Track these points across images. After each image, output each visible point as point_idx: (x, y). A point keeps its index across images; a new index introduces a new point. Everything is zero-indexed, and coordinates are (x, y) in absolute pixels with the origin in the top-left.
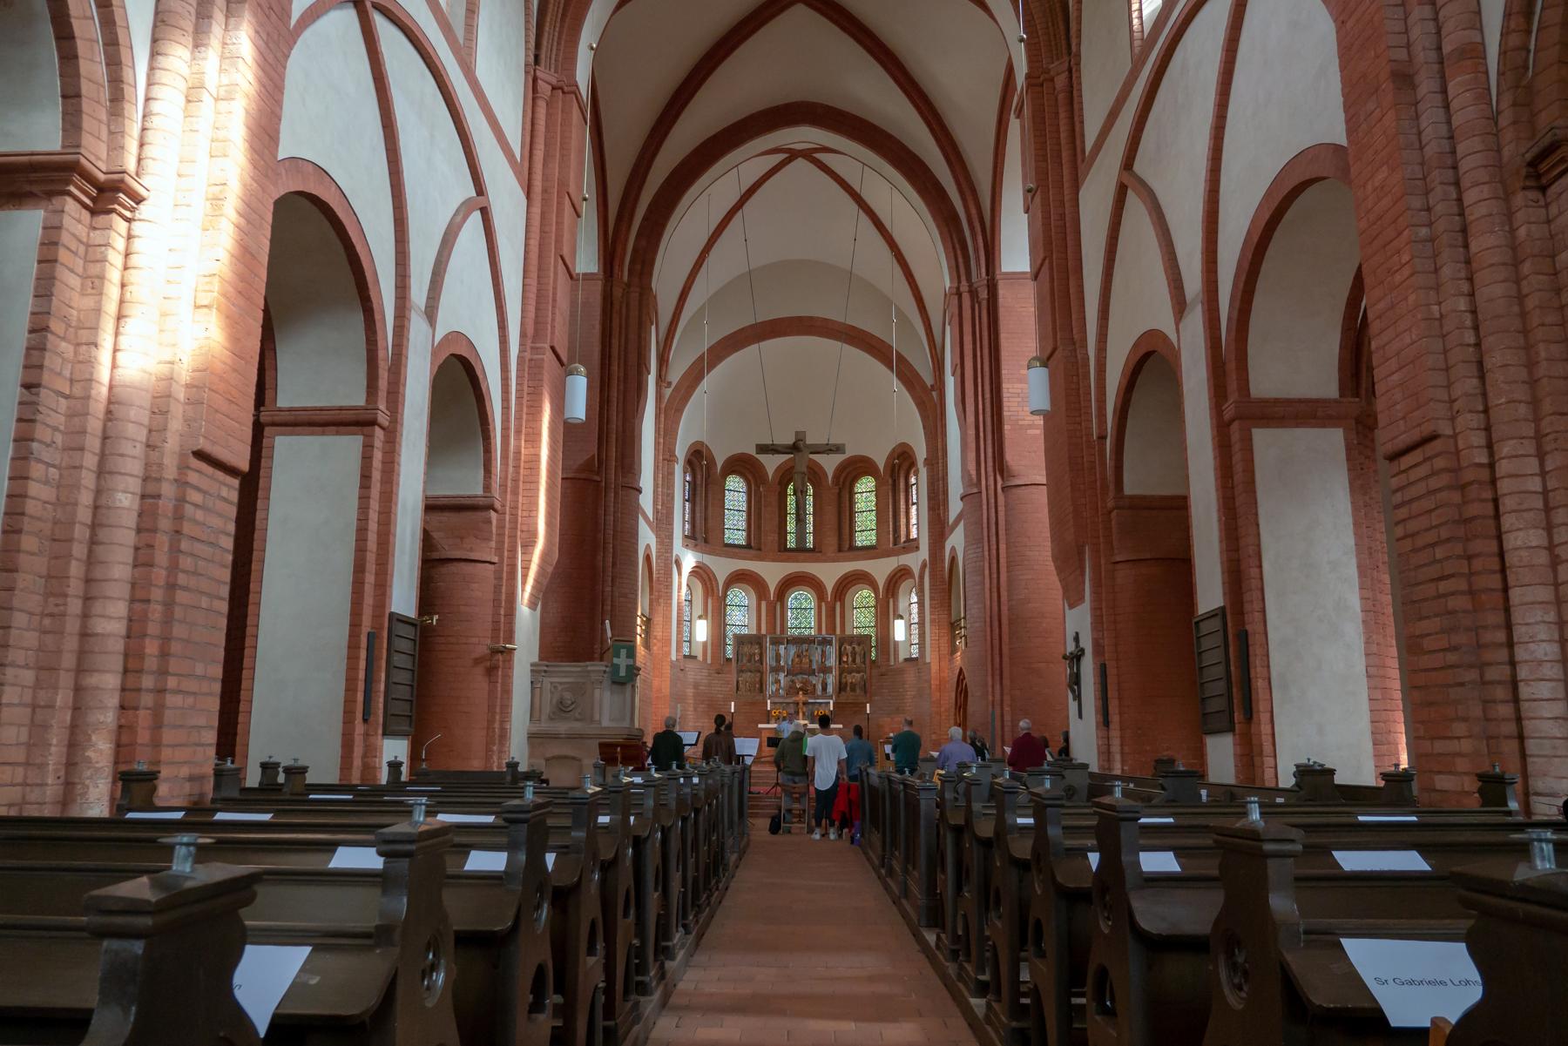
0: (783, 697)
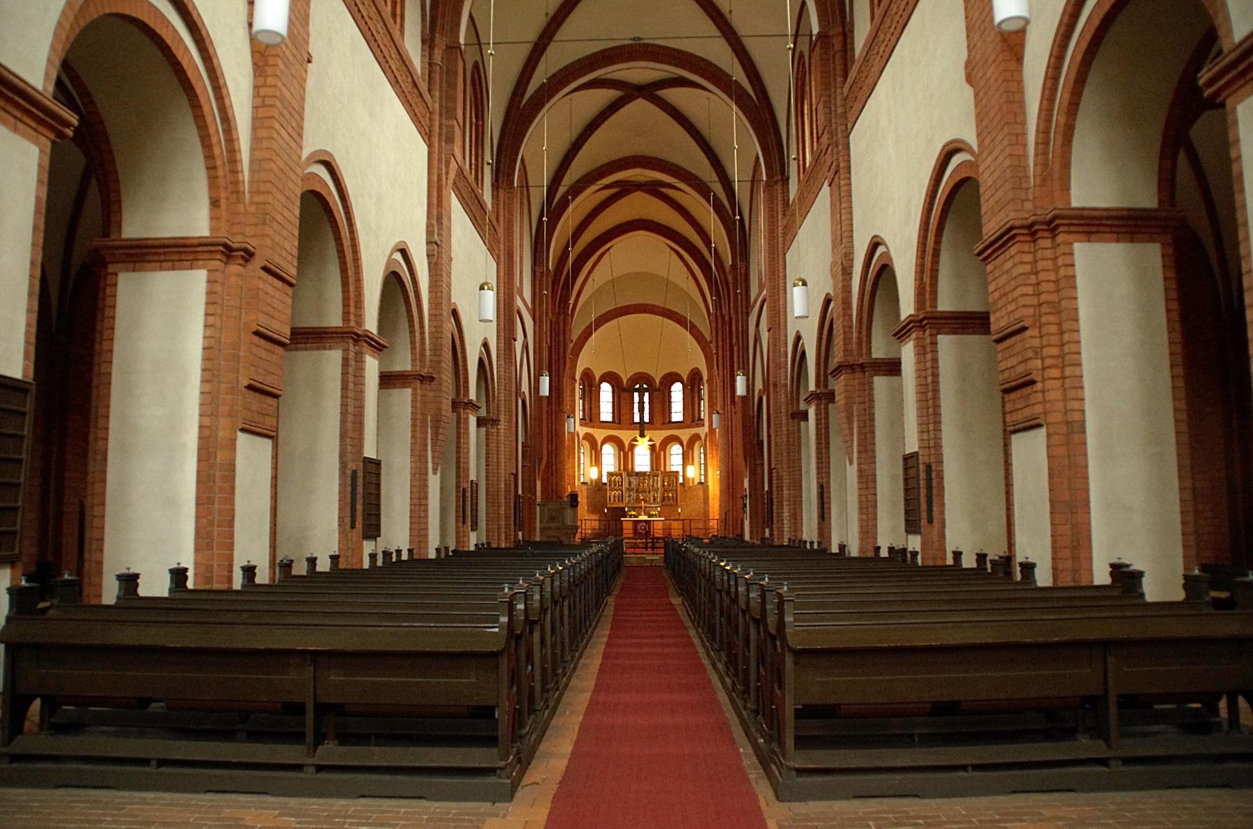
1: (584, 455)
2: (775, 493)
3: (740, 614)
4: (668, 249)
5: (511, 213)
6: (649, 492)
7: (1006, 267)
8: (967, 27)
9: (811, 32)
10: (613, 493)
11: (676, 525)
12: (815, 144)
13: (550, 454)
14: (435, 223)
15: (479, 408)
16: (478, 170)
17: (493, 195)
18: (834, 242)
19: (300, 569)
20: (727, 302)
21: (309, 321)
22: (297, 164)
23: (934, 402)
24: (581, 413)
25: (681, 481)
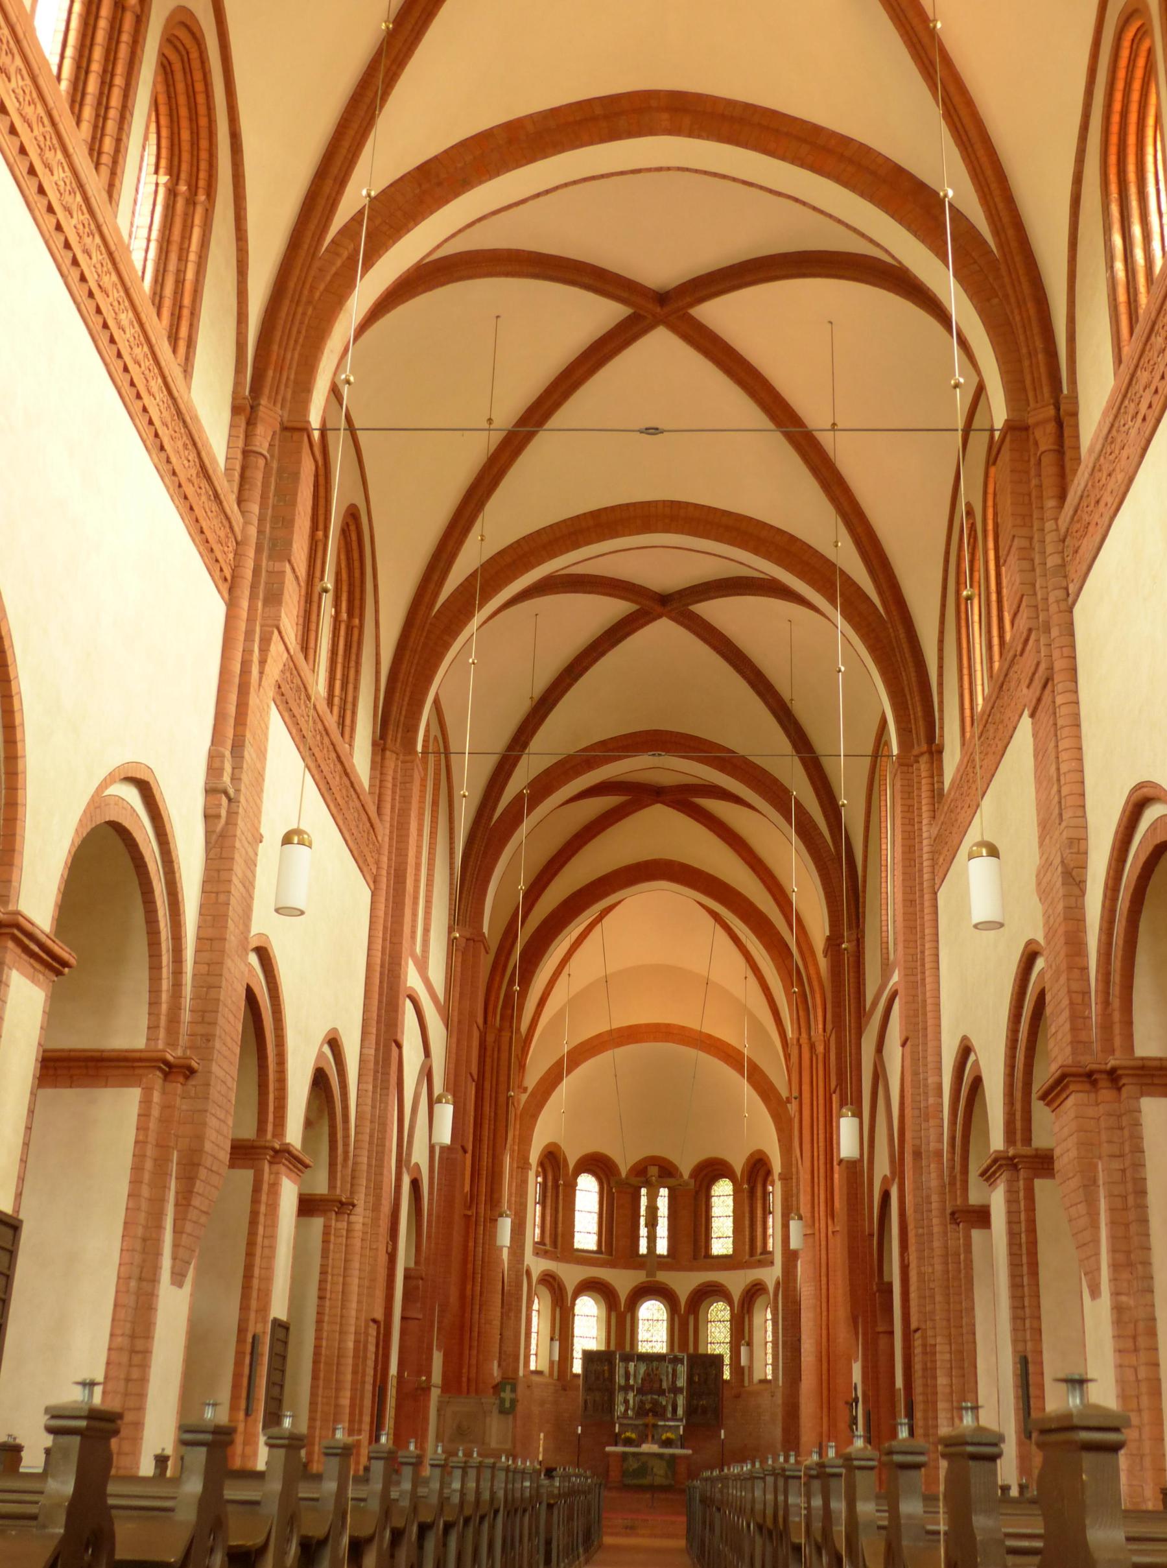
0: (631, 1418)
5: (406, 800)
14: (228, 753)
17: (373, 762)
24: (538, 1231)
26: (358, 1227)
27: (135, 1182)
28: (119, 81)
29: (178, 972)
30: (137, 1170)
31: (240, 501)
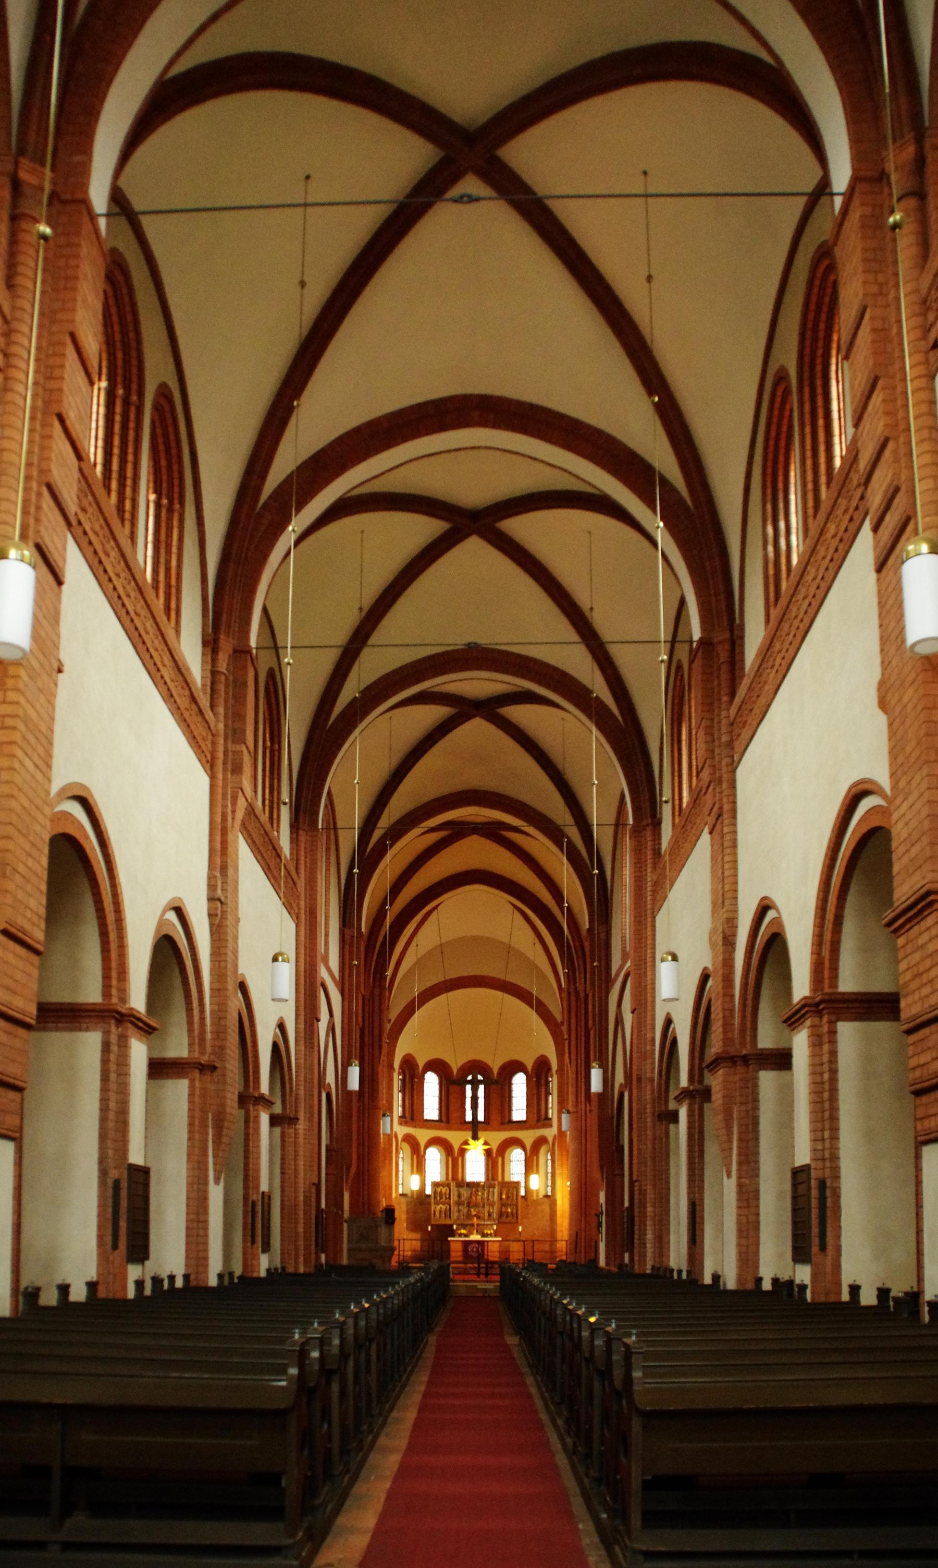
1: (403, 1160)
2: (636, 1210)
3: (584, 1365)
4: (512, 907)
5: (314, 862)
6: (484, 1207)
7: (921, 941)
8: (881, 638)
9: (691, 637)
10: (438, 1207)
11: (516, 1247)
12: (694, 779)
13: (360, 1158)
14: (218, 874)
15: (273, 1104)
16: (273, 805)
17: (291, 838)
18: (714, 903)
19: (49, 1298)
20: (582, 976)
21: (60, 995)
22: (45, 802)
23: (831, 1105)
24: (400, 1109)
25: (522, 1193)
26: (301, 1132)
27: (191, 1132)
28: (130, 457)
29: (202, 1011)
30: (191, 1124)
31: (212, 707)
